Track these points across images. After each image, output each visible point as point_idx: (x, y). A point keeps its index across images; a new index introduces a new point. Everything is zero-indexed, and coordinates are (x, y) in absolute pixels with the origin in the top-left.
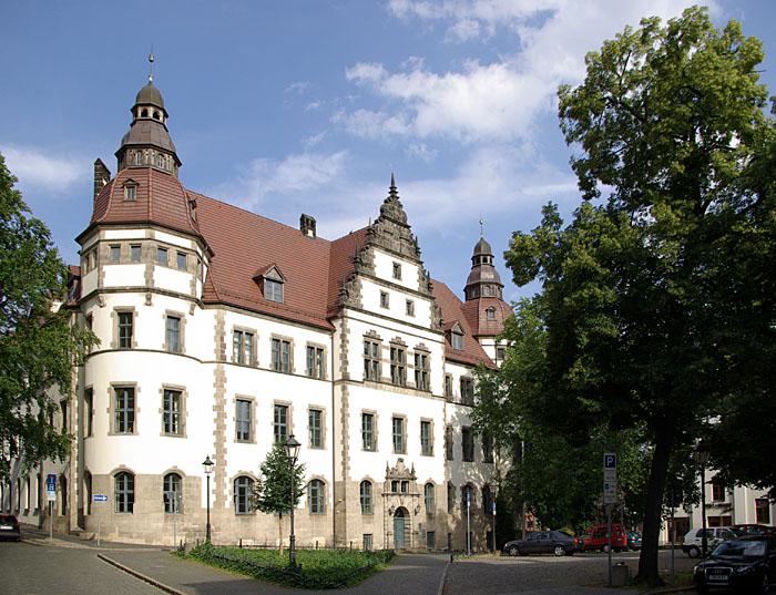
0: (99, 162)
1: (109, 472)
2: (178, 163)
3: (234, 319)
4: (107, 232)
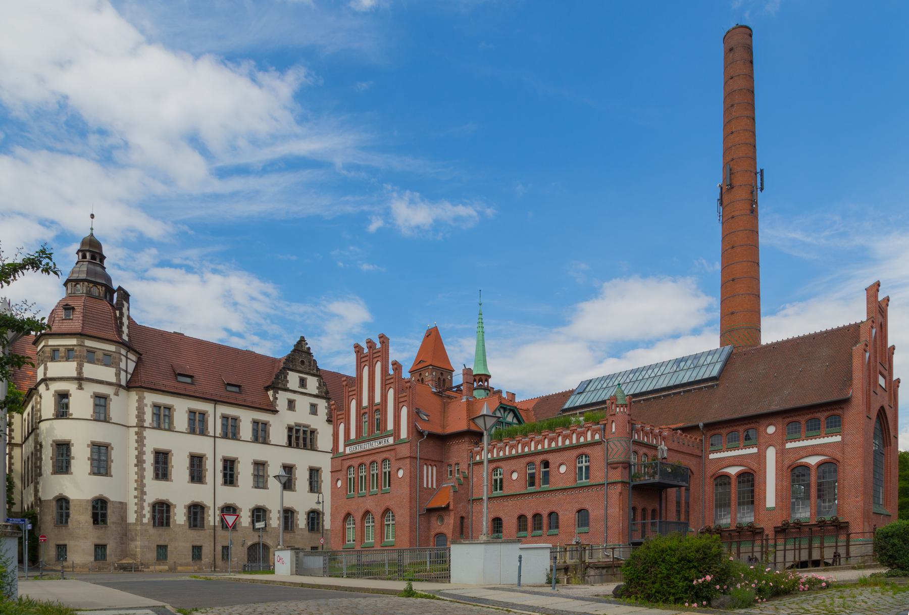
1: (51, 498)
3: (151, 398)
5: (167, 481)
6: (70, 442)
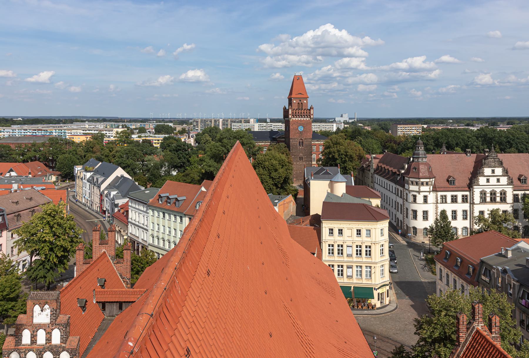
3: (440, 194)
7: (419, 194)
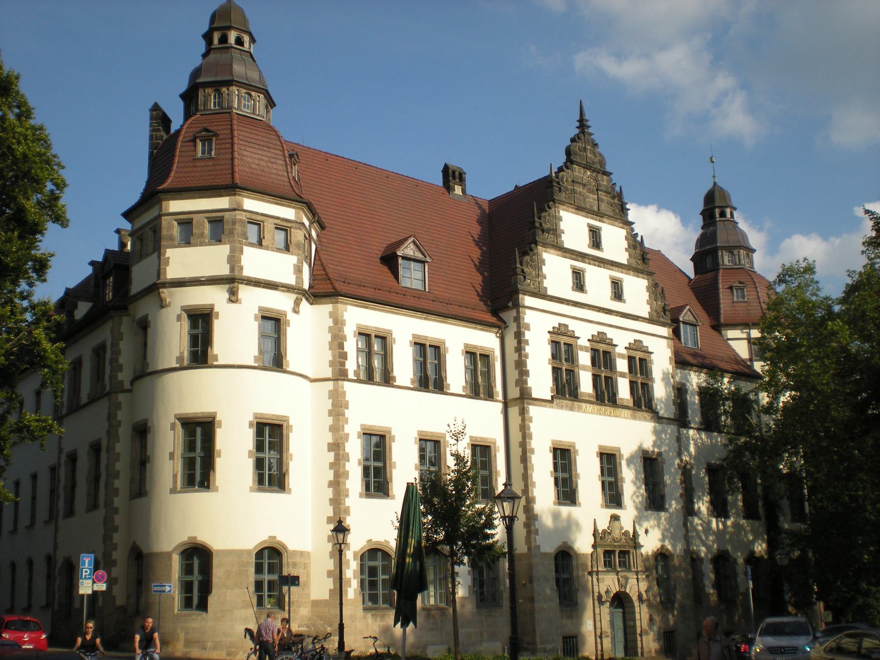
0: (156, 108)
2: (271, 103)
4: (349, 307)
5: (620, 509)
6: (214, 418)
7: (233, 296)
